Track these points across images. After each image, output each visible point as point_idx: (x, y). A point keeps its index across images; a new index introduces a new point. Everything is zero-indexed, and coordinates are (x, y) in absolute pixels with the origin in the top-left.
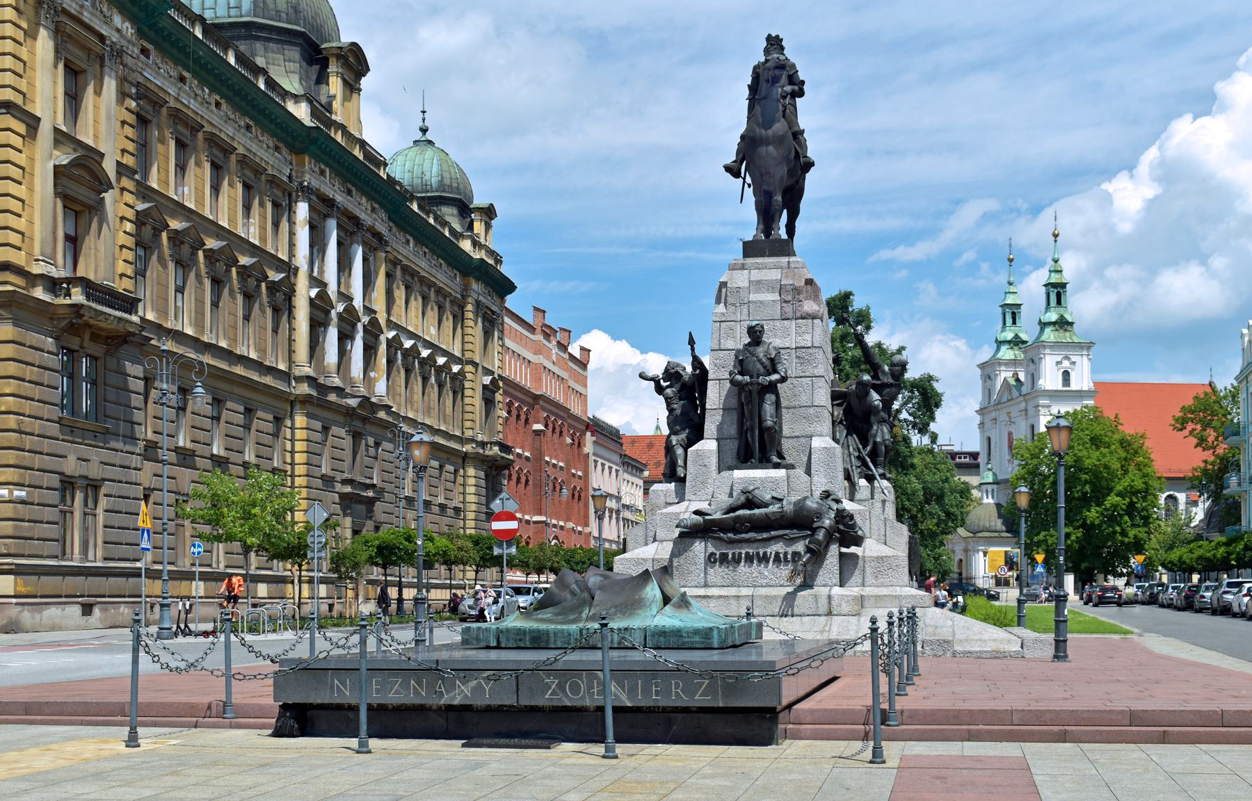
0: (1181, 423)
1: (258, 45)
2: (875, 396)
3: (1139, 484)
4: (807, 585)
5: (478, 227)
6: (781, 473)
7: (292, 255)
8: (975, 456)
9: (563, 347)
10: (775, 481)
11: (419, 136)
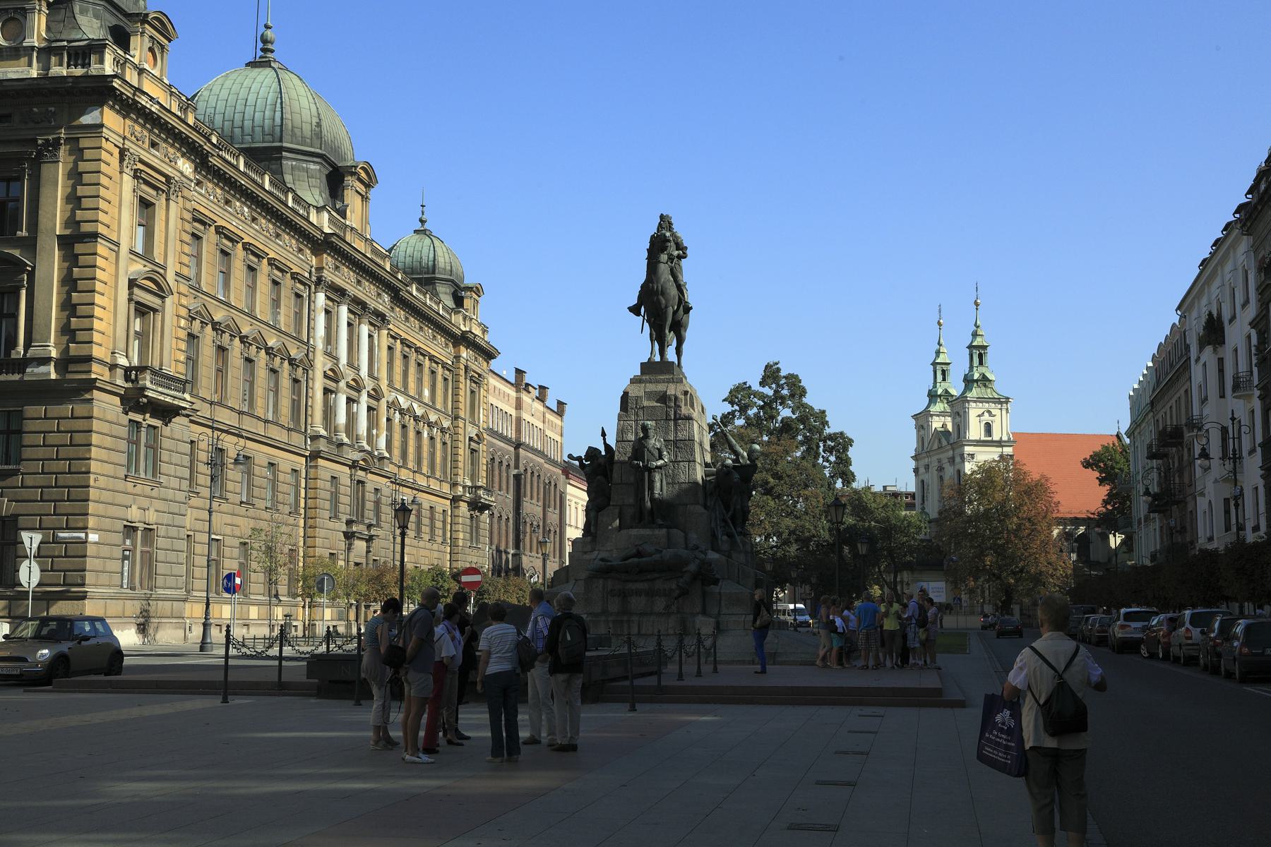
8: (913, 495)
11: (418, 226)
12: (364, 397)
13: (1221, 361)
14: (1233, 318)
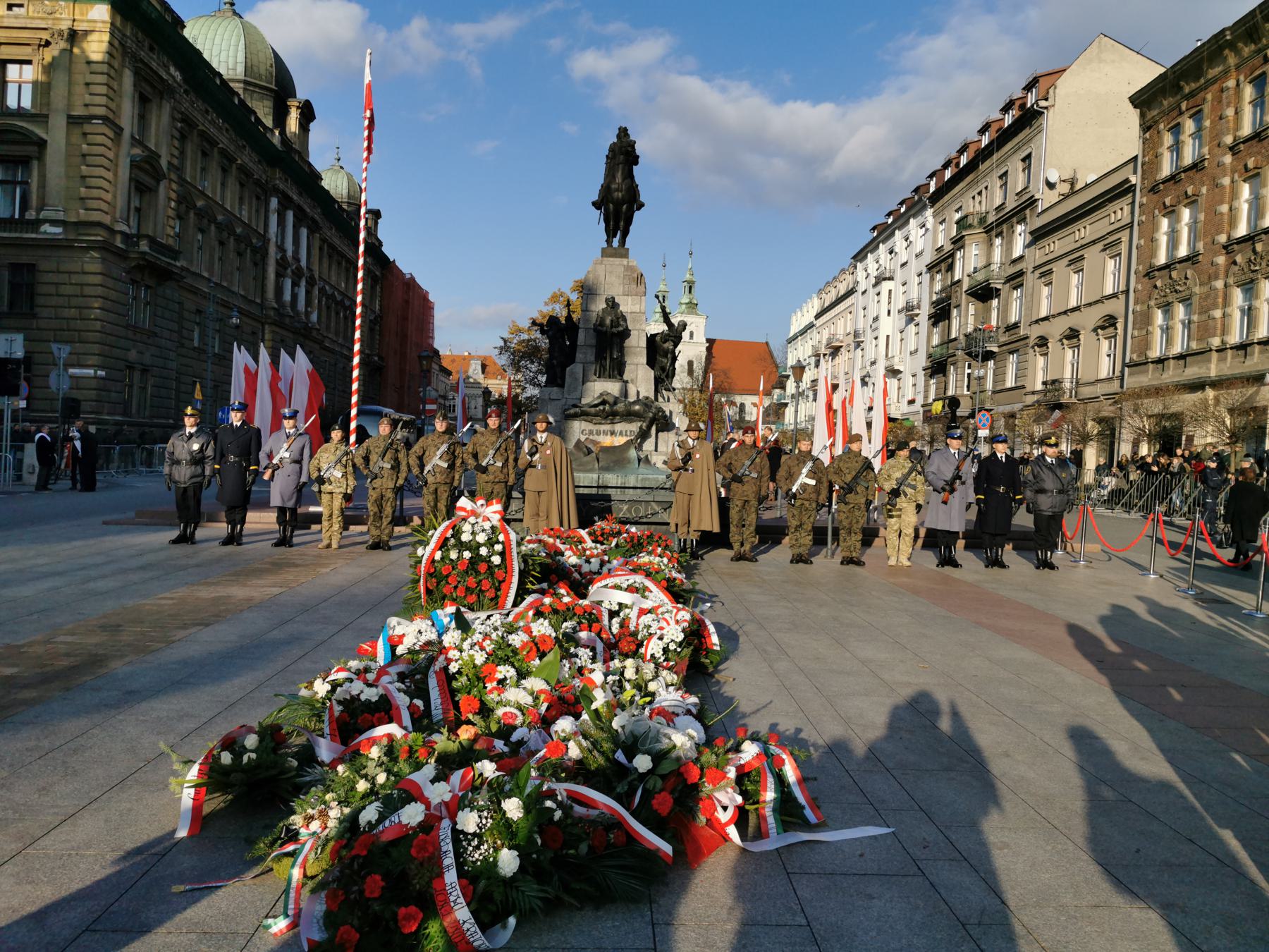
12: (303, 283)
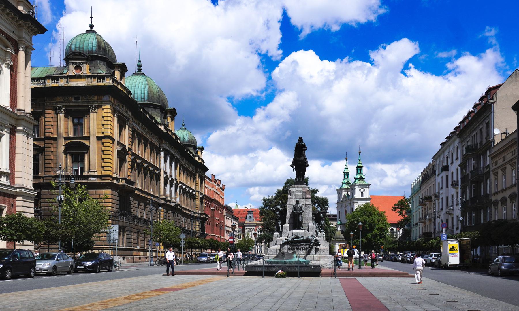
0: (394, 209)
1: (149, 109)
2: (322, 215)
3: (382, 226)
4: (309, 254)
5: (199, 153)
6: (303, 231)
7: (160, 166)
8: (335, 216)
9: (219, 185)
10: (302, 233)
13: (447, 176)
14: (452, 163)
